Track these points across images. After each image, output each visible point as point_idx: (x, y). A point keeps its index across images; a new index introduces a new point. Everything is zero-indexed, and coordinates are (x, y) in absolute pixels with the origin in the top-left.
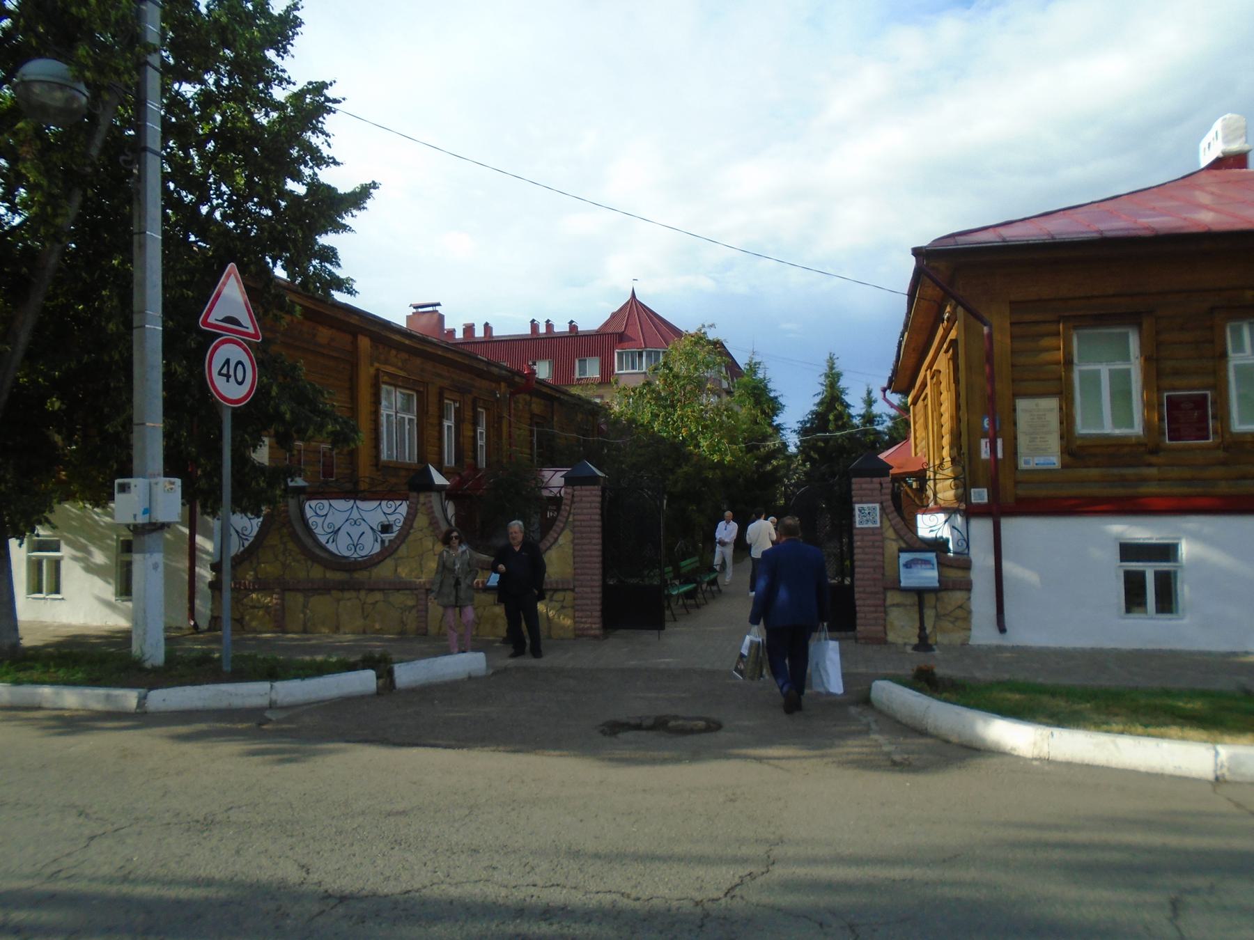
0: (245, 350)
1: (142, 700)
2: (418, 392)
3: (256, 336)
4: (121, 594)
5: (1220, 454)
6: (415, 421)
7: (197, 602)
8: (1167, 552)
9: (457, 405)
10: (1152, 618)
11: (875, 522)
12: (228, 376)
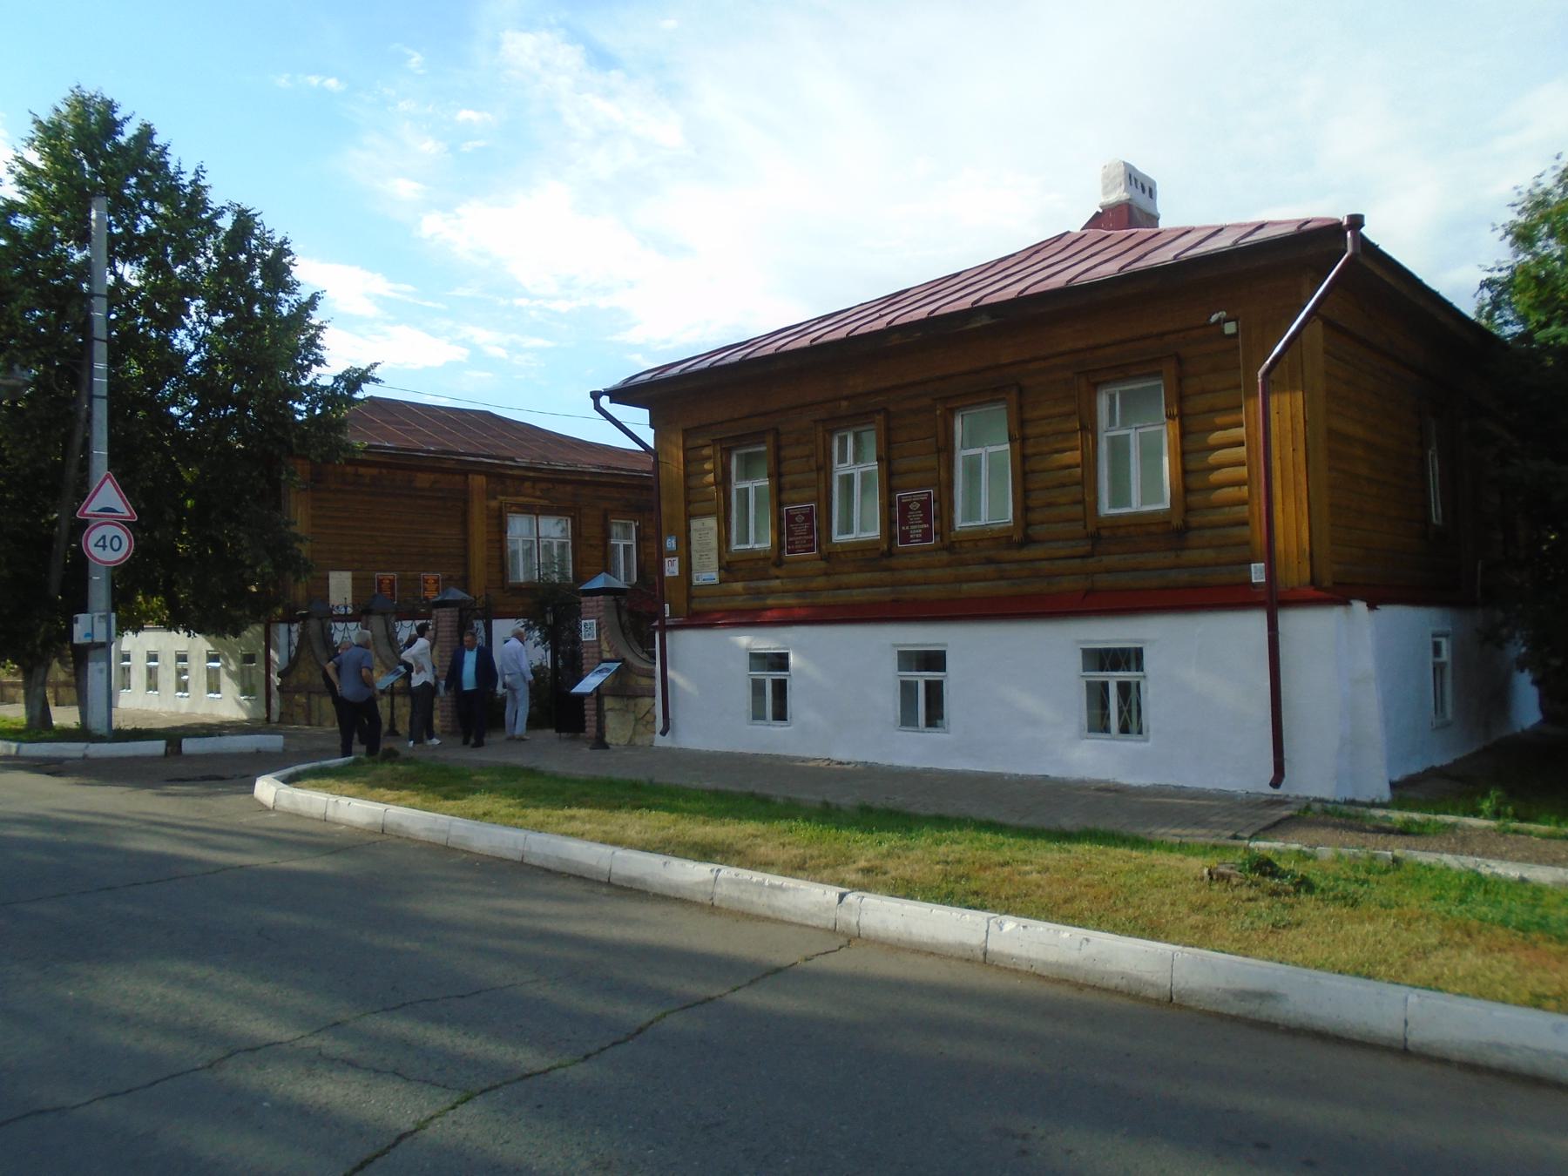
0: (123, 529)
1: (18, 749)
2: (571, 517)
3: (132, 517)
4: (1091, 729)
5: (823, 564)
6: (570, 544)
7: (273, 701)
8: (780, 662)
9: (638, 524)
10: (1114, 739)
11: (585, 637)
12: (104, 547)
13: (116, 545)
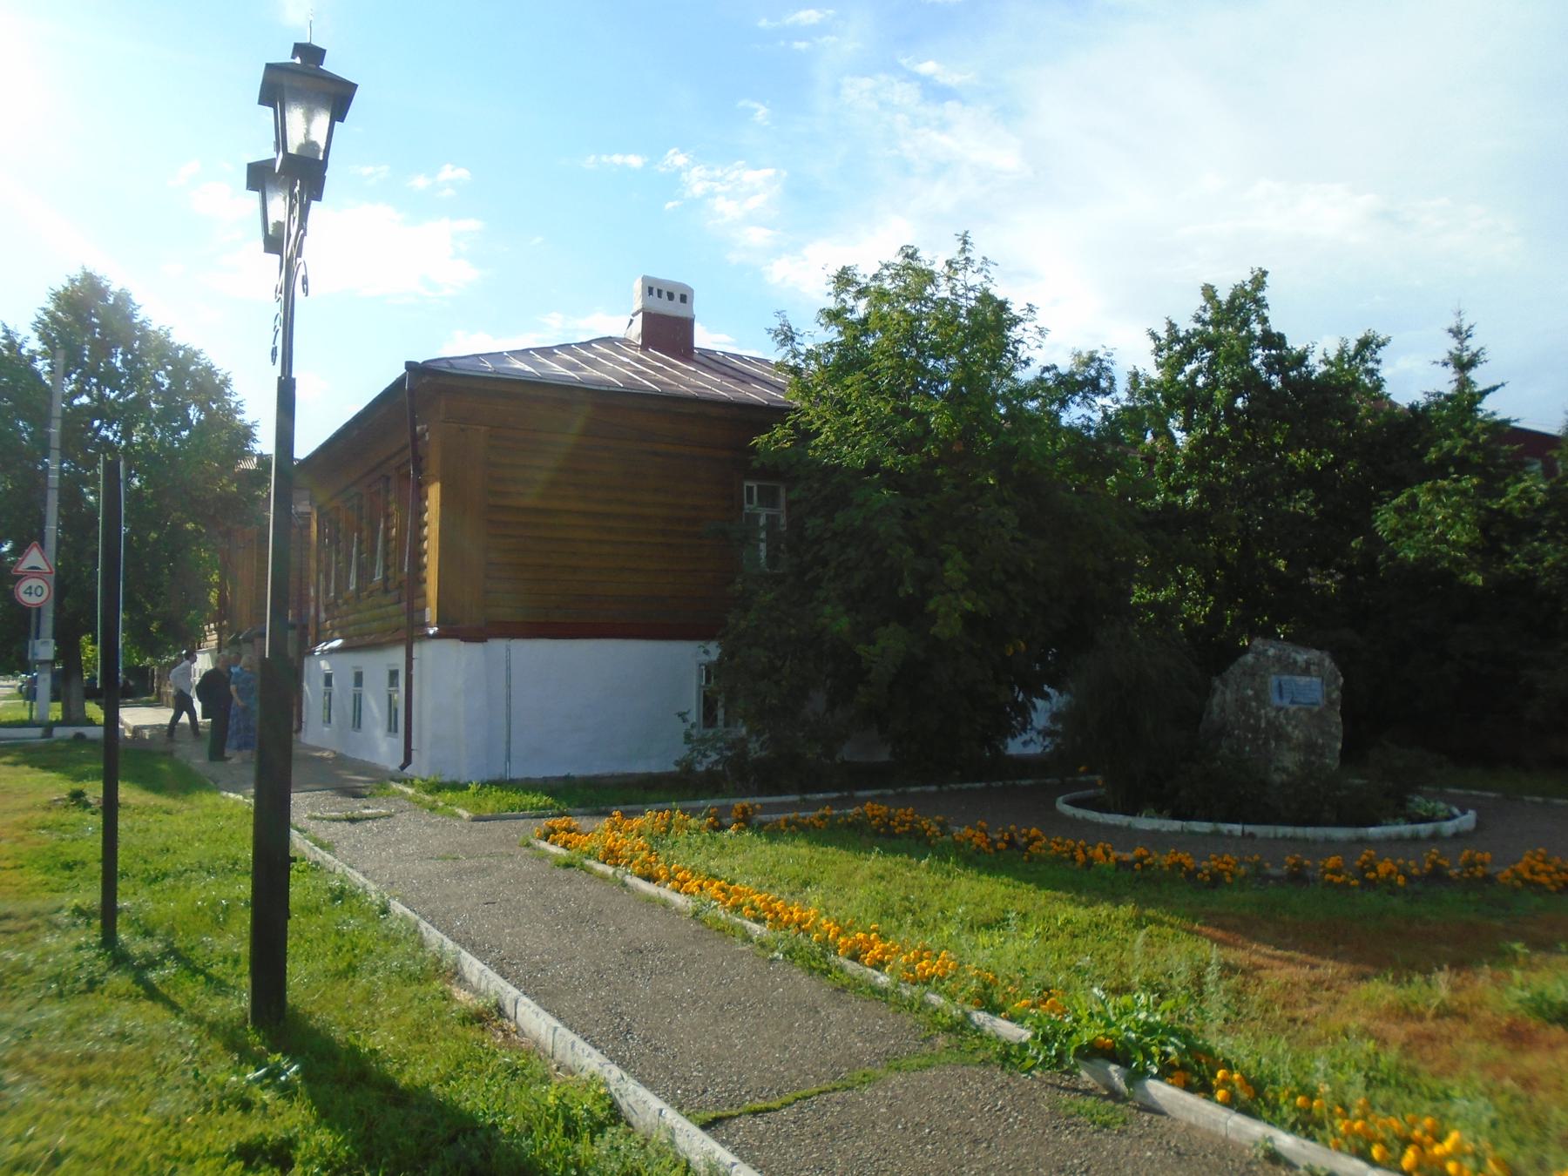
13: (39, 592)
